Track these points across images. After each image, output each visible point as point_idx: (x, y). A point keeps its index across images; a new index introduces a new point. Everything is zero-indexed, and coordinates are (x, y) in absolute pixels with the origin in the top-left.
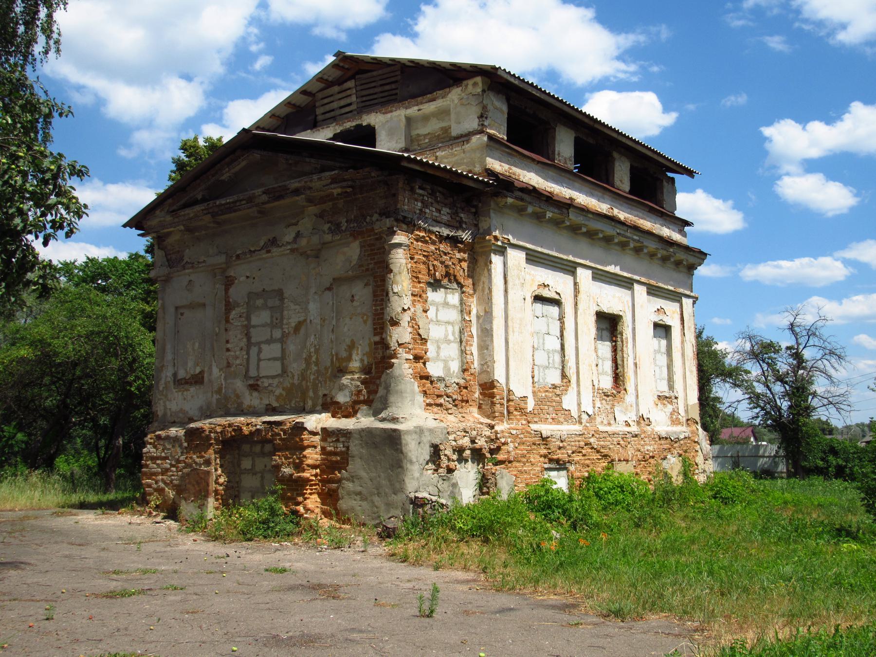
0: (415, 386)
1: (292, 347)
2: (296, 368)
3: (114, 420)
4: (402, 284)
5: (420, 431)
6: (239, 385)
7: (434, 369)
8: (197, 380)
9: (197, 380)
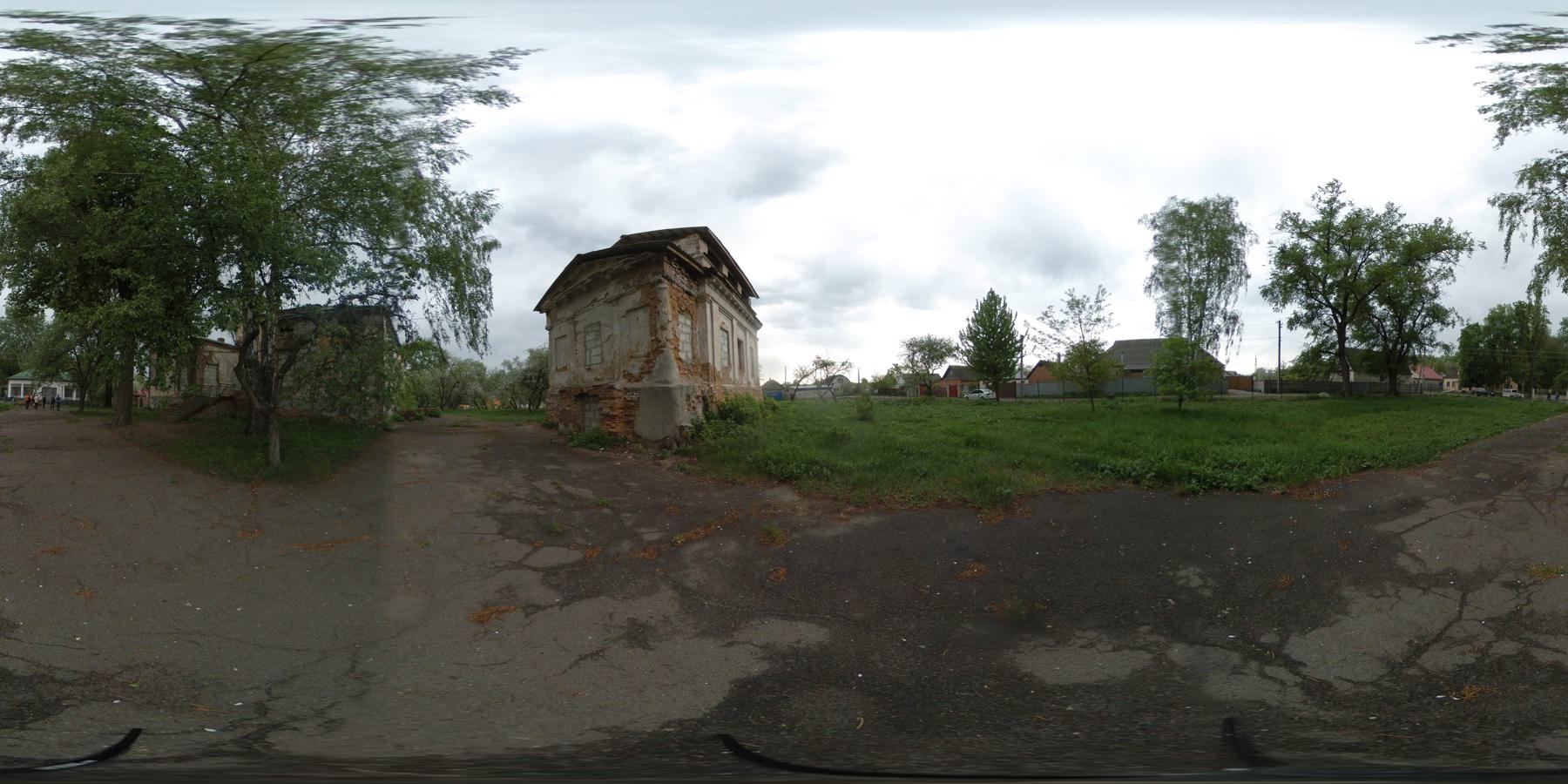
0: (675, 363)
1: (606, 348)
2: (608, 358)
3: (1349, 243)
4: (668, 308)
5: (681, 388)
6: (582, 369)
7: (682, 355)
8: (565, 369)
9: (565, 369)
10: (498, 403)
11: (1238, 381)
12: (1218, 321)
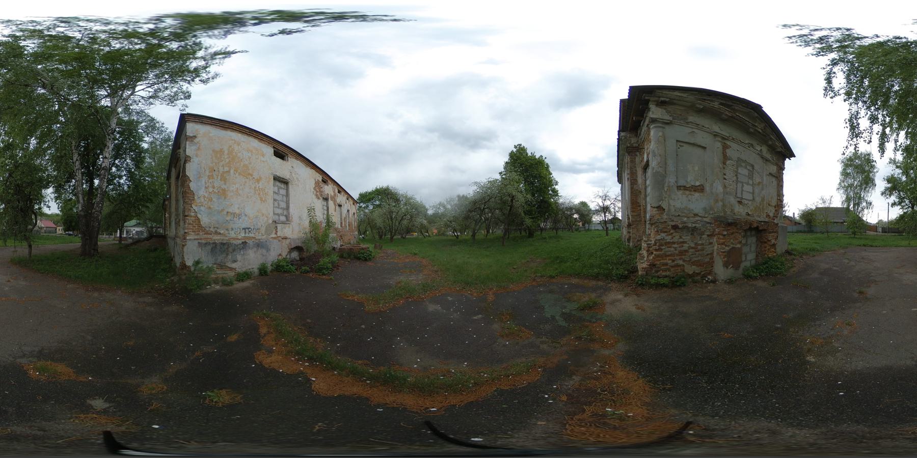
8: (700, 189)
9: (700, 189)
10: (436, 231)
11: (873, 228)
12: (864, 204)
